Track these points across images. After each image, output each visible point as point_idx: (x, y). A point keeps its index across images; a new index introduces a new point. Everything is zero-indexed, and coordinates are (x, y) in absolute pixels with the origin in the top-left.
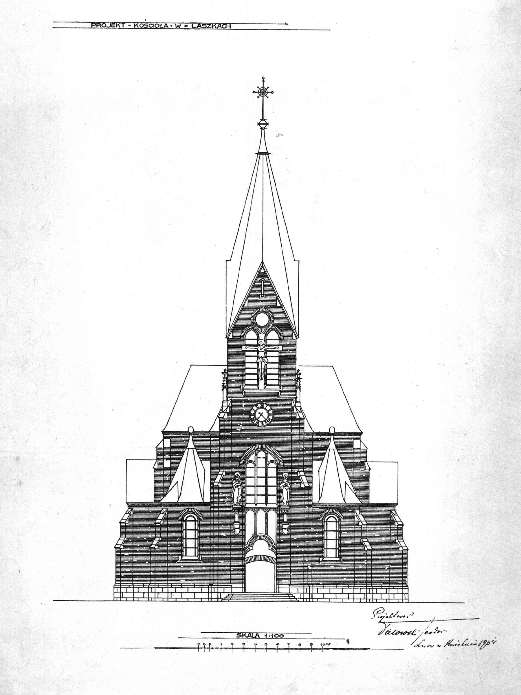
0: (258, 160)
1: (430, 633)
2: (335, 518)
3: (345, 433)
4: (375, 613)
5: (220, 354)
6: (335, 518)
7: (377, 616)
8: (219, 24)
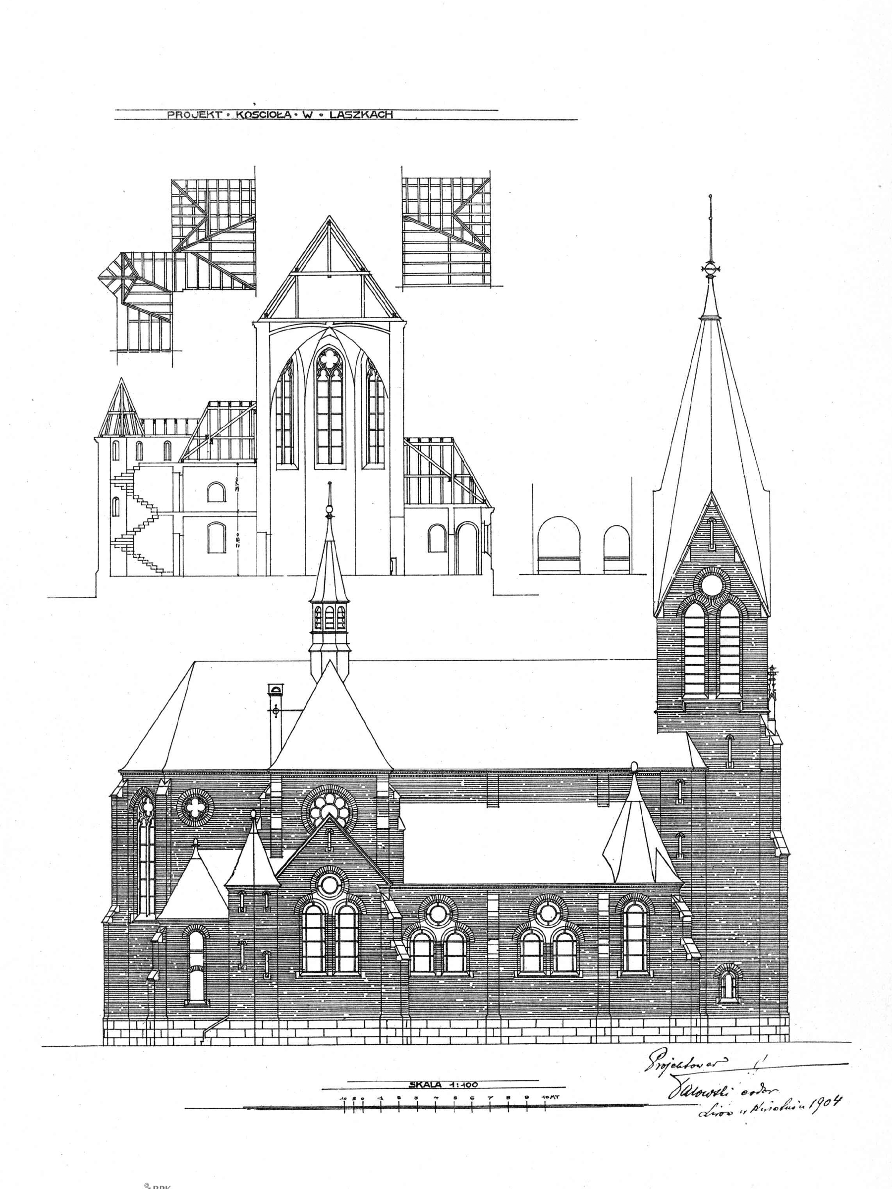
0: (701, 331)
1: (752, 1093)
2: (353, 909)
3: (425, 771)
4: (654, 1057)
5: (645, 640)
6: (353, 909)
7: (656, 1064)
8: (374, 111)
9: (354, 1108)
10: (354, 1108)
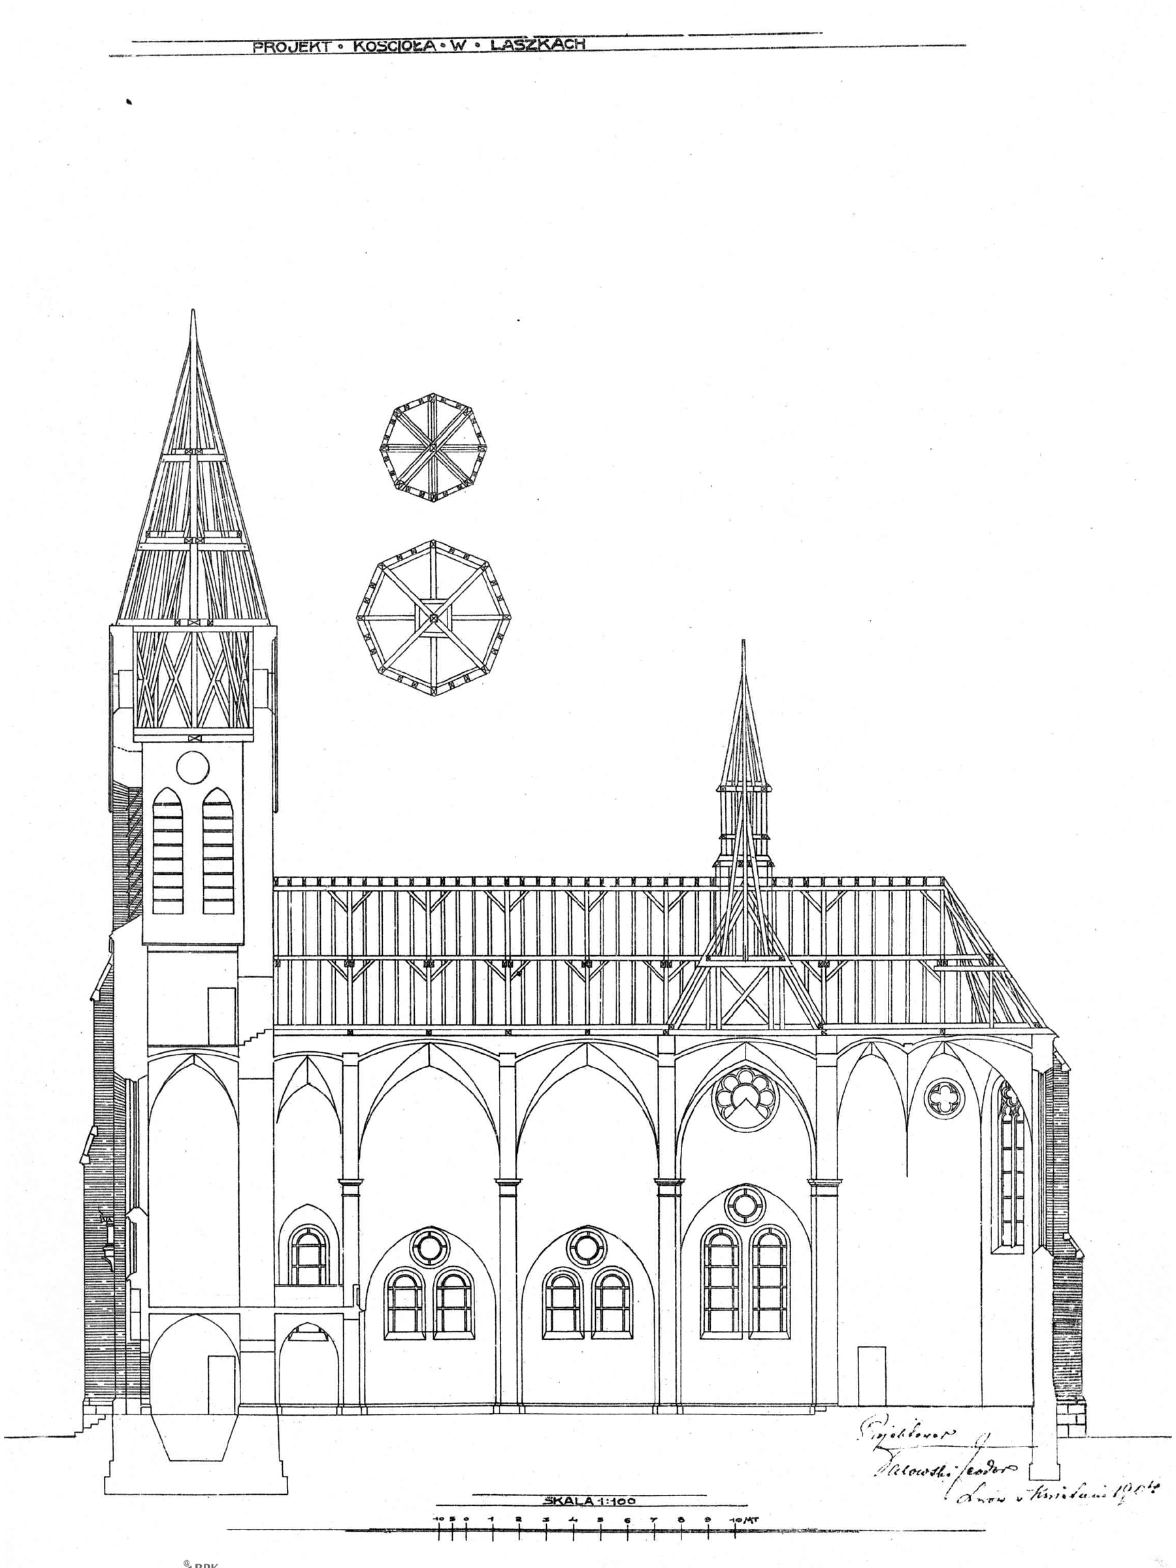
8: (558, 38)
9: (452, 1530)
10: (452, 1530)
